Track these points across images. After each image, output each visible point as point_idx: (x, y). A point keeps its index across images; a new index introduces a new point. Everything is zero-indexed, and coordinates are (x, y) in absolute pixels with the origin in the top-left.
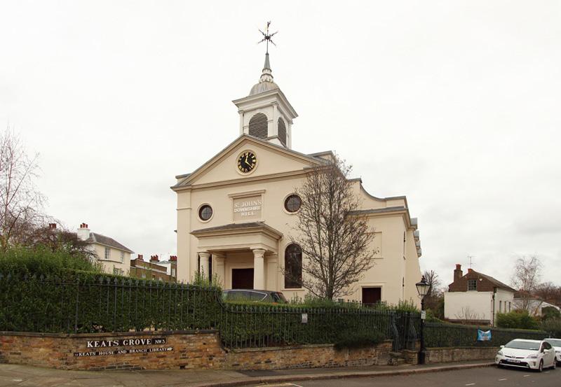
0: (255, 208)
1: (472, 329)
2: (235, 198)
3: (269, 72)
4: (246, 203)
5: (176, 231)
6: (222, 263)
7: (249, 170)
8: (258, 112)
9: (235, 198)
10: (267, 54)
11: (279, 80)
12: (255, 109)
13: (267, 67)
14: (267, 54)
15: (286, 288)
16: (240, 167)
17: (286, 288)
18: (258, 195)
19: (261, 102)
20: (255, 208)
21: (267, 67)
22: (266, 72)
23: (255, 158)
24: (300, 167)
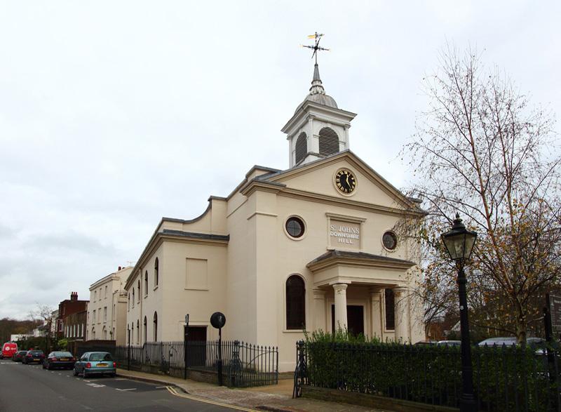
0: (353, 236)
1: (106, 360)
2: (334, 219)
3: (319, 84)
4: (342, 227)
5: (120, 268)
6: (323, 297)
7: (349, 192)
8: (329, 126)
9: (334, 219)
10: (316, 65)
11: (330, 89)
12: (326, 122)
13: (316, 78)
14: (316, 65)
15: (287, 329)
16: (339, 184)
17: (287, 329)
18: (358, 223)
19: (332, 117)
20: (353, 236)
21: (316, 78)
22: (317, 83)
23: (339, 174)
24: (394, 205)
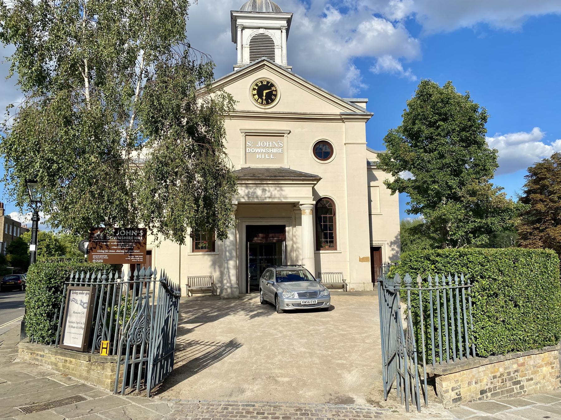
0: (275, 151)
8: (261, 31)
18: (279, 135)
20: (275, 151)
23: (254, 95)
